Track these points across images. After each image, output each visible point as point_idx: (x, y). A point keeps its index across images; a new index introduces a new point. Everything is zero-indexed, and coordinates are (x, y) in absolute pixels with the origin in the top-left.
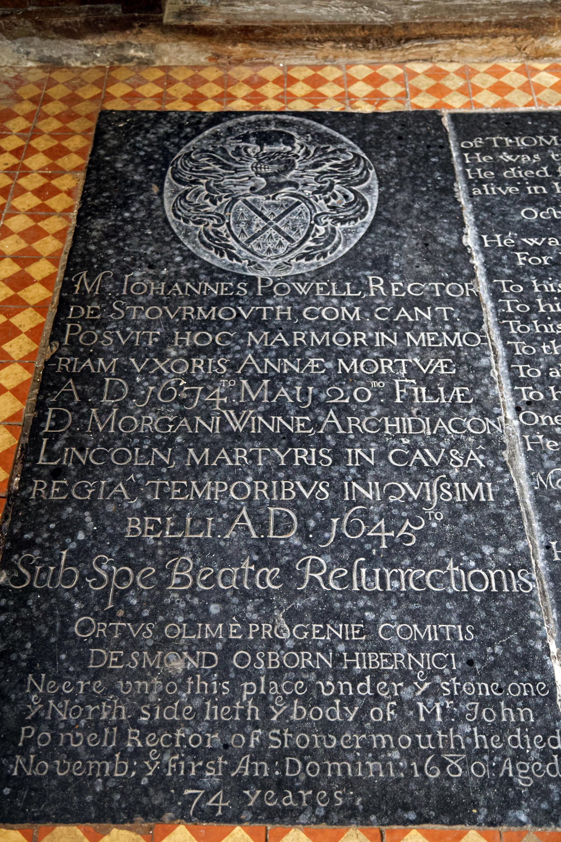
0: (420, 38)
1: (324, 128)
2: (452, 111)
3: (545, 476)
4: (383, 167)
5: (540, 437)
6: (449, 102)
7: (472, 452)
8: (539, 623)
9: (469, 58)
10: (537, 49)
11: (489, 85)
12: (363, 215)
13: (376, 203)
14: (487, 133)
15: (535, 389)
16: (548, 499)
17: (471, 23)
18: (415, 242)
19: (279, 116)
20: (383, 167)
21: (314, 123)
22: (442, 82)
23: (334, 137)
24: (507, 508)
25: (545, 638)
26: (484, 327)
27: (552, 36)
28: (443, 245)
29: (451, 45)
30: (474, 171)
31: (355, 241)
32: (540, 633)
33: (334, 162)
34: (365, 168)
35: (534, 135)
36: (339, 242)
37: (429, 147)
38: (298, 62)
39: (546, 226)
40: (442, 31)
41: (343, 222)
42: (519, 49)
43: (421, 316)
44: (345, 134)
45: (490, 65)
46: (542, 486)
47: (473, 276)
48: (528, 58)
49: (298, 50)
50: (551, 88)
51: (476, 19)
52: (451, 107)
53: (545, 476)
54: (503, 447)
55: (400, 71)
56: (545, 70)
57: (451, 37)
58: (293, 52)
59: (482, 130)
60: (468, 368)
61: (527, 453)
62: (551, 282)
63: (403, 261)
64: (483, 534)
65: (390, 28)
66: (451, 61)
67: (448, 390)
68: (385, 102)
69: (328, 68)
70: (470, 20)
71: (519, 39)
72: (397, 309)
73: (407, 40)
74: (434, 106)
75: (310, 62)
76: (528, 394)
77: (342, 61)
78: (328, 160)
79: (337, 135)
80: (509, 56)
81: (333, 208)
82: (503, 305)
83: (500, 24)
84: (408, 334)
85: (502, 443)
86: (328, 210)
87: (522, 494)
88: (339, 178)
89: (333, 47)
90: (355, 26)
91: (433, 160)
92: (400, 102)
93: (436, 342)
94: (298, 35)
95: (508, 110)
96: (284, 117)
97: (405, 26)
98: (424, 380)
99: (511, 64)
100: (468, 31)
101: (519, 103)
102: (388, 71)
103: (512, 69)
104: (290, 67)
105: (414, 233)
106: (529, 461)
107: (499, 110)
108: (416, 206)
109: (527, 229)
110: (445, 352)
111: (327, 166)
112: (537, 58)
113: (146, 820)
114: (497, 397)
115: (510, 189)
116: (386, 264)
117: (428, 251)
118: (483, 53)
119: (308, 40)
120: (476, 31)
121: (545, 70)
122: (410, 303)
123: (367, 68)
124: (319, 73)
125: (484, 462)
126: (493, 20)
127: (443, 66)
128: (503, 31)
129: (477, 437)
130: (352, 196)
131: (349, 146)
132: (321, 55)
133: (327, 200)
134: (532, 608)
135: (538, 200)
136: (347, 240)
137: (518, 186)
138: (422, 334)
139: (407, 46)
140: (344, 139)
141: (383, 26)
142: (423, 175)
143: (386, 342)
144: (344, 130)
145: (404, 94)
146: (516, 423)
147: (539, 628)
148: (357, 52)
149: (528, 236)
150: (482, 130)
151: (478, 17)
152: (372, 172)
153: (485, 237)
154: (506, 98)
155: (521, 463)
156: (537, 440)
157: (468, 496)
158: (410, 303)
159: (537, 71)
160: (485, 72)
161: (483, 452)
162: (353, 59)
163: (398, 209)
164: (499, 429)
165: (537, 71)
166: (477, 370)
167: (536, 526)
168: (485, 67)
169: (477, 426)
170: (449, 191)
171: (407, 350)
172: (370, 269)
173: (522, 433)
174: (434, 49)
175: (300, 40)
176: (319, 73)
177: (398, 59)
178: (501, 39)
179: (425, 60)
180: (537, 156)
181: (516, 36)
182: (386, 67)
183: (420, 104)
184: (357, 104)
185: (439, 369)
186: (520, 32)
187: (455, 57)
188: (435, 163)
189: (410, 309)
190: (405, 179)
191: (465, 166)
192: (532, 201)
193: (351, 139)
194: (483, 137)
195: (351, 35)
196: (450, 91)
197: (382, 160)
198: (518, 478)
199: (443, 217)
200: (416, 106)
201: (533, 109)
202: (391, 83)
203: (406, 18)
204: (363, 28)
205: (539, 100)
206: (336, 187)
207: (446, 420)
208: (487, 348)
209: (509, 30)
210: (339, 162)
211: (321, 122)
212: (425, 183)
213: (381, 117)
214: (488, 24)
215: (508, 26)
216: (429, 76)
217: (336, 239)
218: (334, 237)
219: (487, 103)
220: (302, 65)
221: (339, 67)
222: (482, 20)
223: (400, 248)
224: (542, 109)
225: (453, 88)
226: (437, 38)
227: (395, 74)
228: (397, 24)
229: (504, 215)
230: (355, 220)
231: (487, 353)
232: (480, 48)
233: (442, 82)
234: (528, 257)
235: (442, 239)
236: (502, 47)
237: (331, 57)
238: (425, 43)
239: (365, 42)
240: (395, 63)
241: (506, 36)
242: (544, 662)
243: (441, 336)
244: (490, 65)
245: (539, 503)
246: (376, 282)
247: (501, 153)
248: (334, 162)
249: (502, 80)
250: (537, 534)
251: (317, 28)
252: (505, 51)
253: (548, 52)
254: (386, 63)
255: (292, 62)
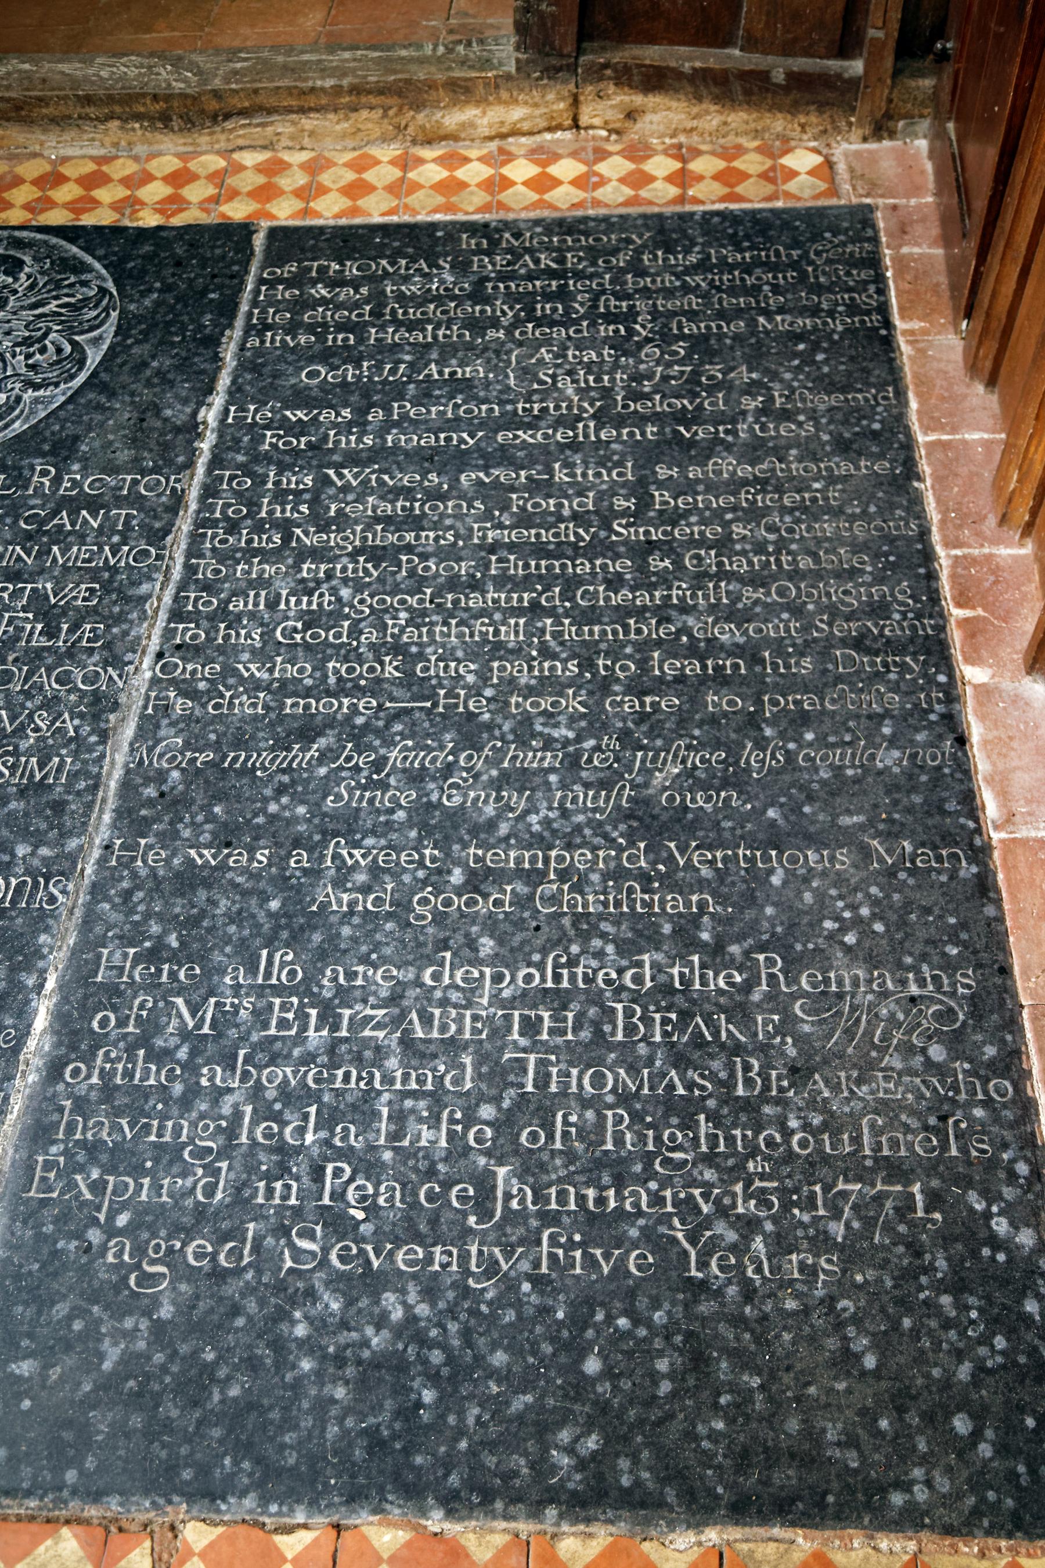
0: (243, 113)
1: (75, 249)
2: (275, 223)
3: (150, 750)
4: (132, 307)
5: (172, 695)
6: (274, 211)
7: (66, 715)
8: (45, 951)
9: (328, 143)
10: (422, 128)
11: (342, 183)
12: (72, 377)
13: (98, 359)
14: (309, 255)
15: (197, 627)
16: (140, 781)
17: (313, 89)
18: (127, 416)
19: (17, 233)
20: (132, 307)
21: (63, 243)
22: (274, 180)
23: (82, 263)
24: (79, 793)
25: (45, 971)
26: (169, 539)
27: (438, 107)
28: (166, 420)
29: (294, 123)
30: (264, 311)
31: (43, 414)
32: (41, 964)
33: (67, 300)
34: (106, 310)
35: (374, 259)
36: (18, 417)
37: (214, 276)
38: (78, 152)
39: (327, 392)
40: (273, 102)
41: (36, 387)
42: (398, 127)
43: (85, 522)
44: (99, 259)
45: (356, 154)
46: (141, 762)
47: (190, 464)
48: (414, 142)
49: (73, 134)
50: (432, 187)
51: (319, 83)
52: (274, 217)
53: (150, 750)
54: (116, 706)
55: (222, 163)
56: (434, 160)
57: (289, 110)
58: (67, 136)
59: (303, 250)
60: (118, 594)
61: (142, 717)
62: (295, 473)
63: (97, 444)
64: (27, 829)
65: (194, 98)
66: (302, 149)
67: (74, 628)
68: (181, 210)
69: (121, 161)
70: (310, 84)
71: (391, 113)
72: (55, 513)
73: (227, 117)
74: (249, 216)
75: (94, 152)
76: (187, 632)
77: (140, 149)
78: (56, 298)
79: (89, 259)
80: (385, 139)
81: (33, 367)
82: (211, 509)
83: (356, 90)
84: (55, 548)
85: (116, 703)
86: (23, 371)
87: (109, 774)
88: (62, 322)
89: (122, 128)
90: (144, 95)
91: (212, 296)
92: (204, 210)
93: (89, 561)
94: (63, 110)
95: (358, 221)
96: (25, 234)
97: (216, 94)
98: (45, 614)
99: (386, 153)
100: (312, 101)
101: (376, 210)
102: (203, 165)
103: (385, 159)
104: (65, 160)
105: (133, 402)
106: (140, 728)
107: (343, 222)
108: (155, 364)
109: (300, 398)
110: (94, 575)
111: (52, 306)
112: (429, 142)
113: (14, 1078)
114: (139, 638)
115: (302, 339)
116: (70, 449)
117: (141, 429)
118: (344, 136)
119: (80, 117)
120: (324, 101)
121: (434, 160)
122: (73, 505)
123: (176, 160)
124: (104, 168)
125: (76, 729)
126: (345, 82)
127: (286, 156)
128: (364, 100)
129: (83, 694)
130: (68, 349)
131: (100, 277)
132: (107, 140)
133: (28, 356)
134: (47, 929)
135: (334, 355)
136: (32, 412)
137: (315, 334)
138: (75, 549)
139: (229, 125)
140: (97, 265)
141: (183, 96)
142: (186, 318)
143: (19, 559)
144: (101, 252)
145: (216, 200)
146: (148, 675)
147: (43, 957)
148: (159, 136)
149: (293, 408)
150: (303, 250)
151: (323, 78)
152: (114, 314)
153: (233, 409)
154: (360, 203)
155: (129, 731)
156: (167, 698)
157: (32, 775)
158: (73, 505)
159: (421, 161)
160: (345, 165)
161: (81, 716)
162: (156, 148)
163: (126, 368)
164: (120, 684)
165: (421, 161)
166: (128, 600)
167: (107, 818)
168: (348, 156)
169: (91, 679)
170: (213, 342)
171: (42, 571)
172: (43, 455)
173: (150, 689)
174: (270, 129)
175: (70, 117)
176: (104, 168)
177: (222, 145)
178: (364, 114)
179: (265, 147)
180: (364, 291)
181: (386, 109)
182: (203, 158)
183: (230, 214)
184: (141, 214)
185: (75, 598)
186: (389, 101)
187: (306, 141)
188: (212, 300)
189: (74, 513)
190: (157, 325)
191: (255, 303)
192: (326, 356)
193: (105, 267)
194: (299, 261)
195: (142, 109)
196: (283, 192)
197: (137, 296)
198: (114, 751)
199: (186, 381)
200: (223, 215)
201: (395, 219)
202: (203, 181)
203: (217, 83)
204: (155, 98)
205: (406, 206)
206: (53, 336)
207: (49, 670)
208: (157, 569)
209: (373, 100)
210: (72, 300)
211: (72, 241)
212: (183, 328)
213: (164, 234)
214: (338, 90)
215: (369, 92)
216: (260, 171)
217: (17, 412)
218: (13, 409)
219: (329, 210)
220: (83, 157)
221: (136, 159)
222: (329, 83)
223: (102, 424)
224: (407, 218)
225: (287, 189)
226: (270, 111)
227: (212, 169)
228: (205, 92)
229: (275, 377)
230: (57, 385)
231: (155, 576)
232: (338, 127)
233: (274, 180)
234: (280, 437)
235: (168, 412)
236: (370, 126)
237: (123, 143)
238: (255, 121)
239: (165, 119)
240: (218, 153)
241: (372, 108)
242: (28, 1002)
243: (101, 550)
244: (356, 154)
245: (126, 785)
246: (44, 473)
247: (314, 286)
248: (67, 300)
249: (364, 176)
250: (103, 829)
251: (88, 100)
252: (377, 132)
253: (442, 132)
254: (201, 153)
255: (69, 152)
